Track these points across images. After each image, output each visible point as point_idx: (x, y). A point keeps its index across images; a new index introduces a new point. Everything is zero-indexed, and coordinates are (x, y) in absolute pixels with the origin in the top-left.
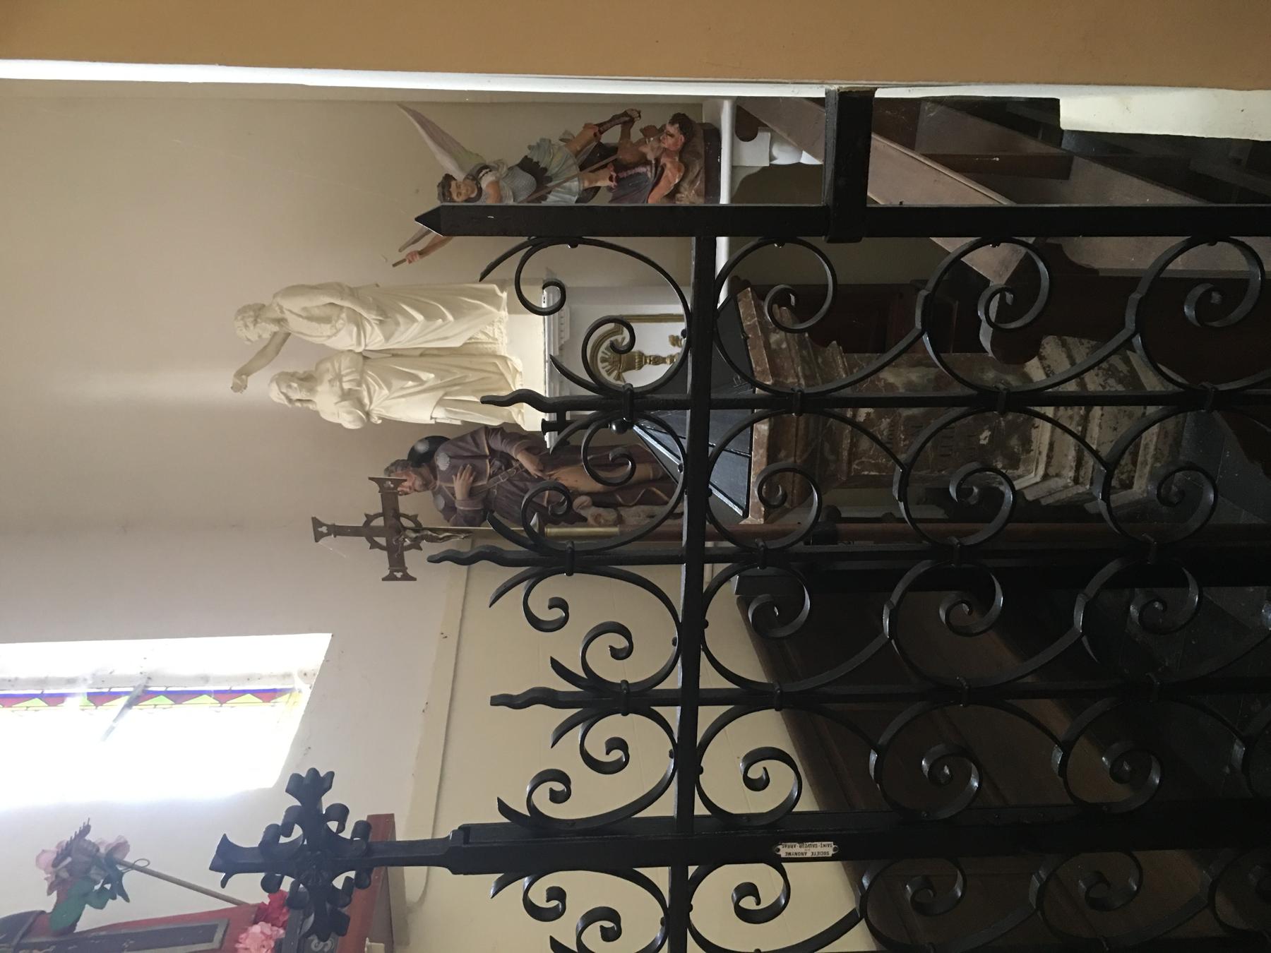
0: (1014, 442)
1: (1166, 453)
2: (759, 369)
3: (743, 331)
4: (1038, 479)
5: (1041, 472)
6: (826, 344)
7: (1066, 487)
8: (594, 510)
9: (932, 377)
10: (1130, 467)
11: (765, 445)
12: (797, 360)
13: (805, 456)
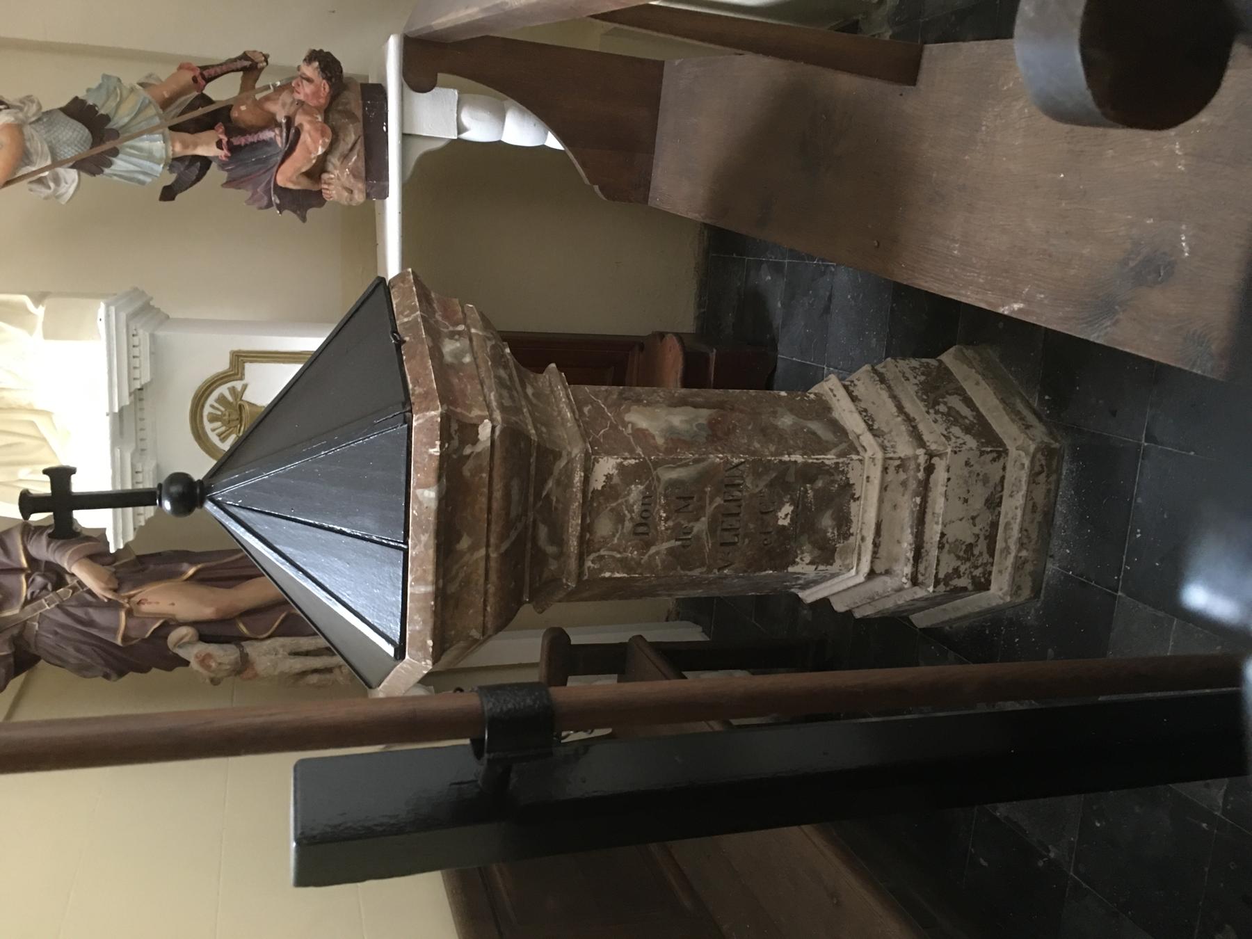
0: (827, 522)
1: (1034, 536)
2: (418, 390)
3: (395, 331)
4: (861, 579)
5: (865, 568)
6: (540, 368)
7: (900, 590)
8: (202, 648)
9: (703, 421)
10: (986, 557)
11: (432, 527)
12: (490, 382)
13: (504, 547)
